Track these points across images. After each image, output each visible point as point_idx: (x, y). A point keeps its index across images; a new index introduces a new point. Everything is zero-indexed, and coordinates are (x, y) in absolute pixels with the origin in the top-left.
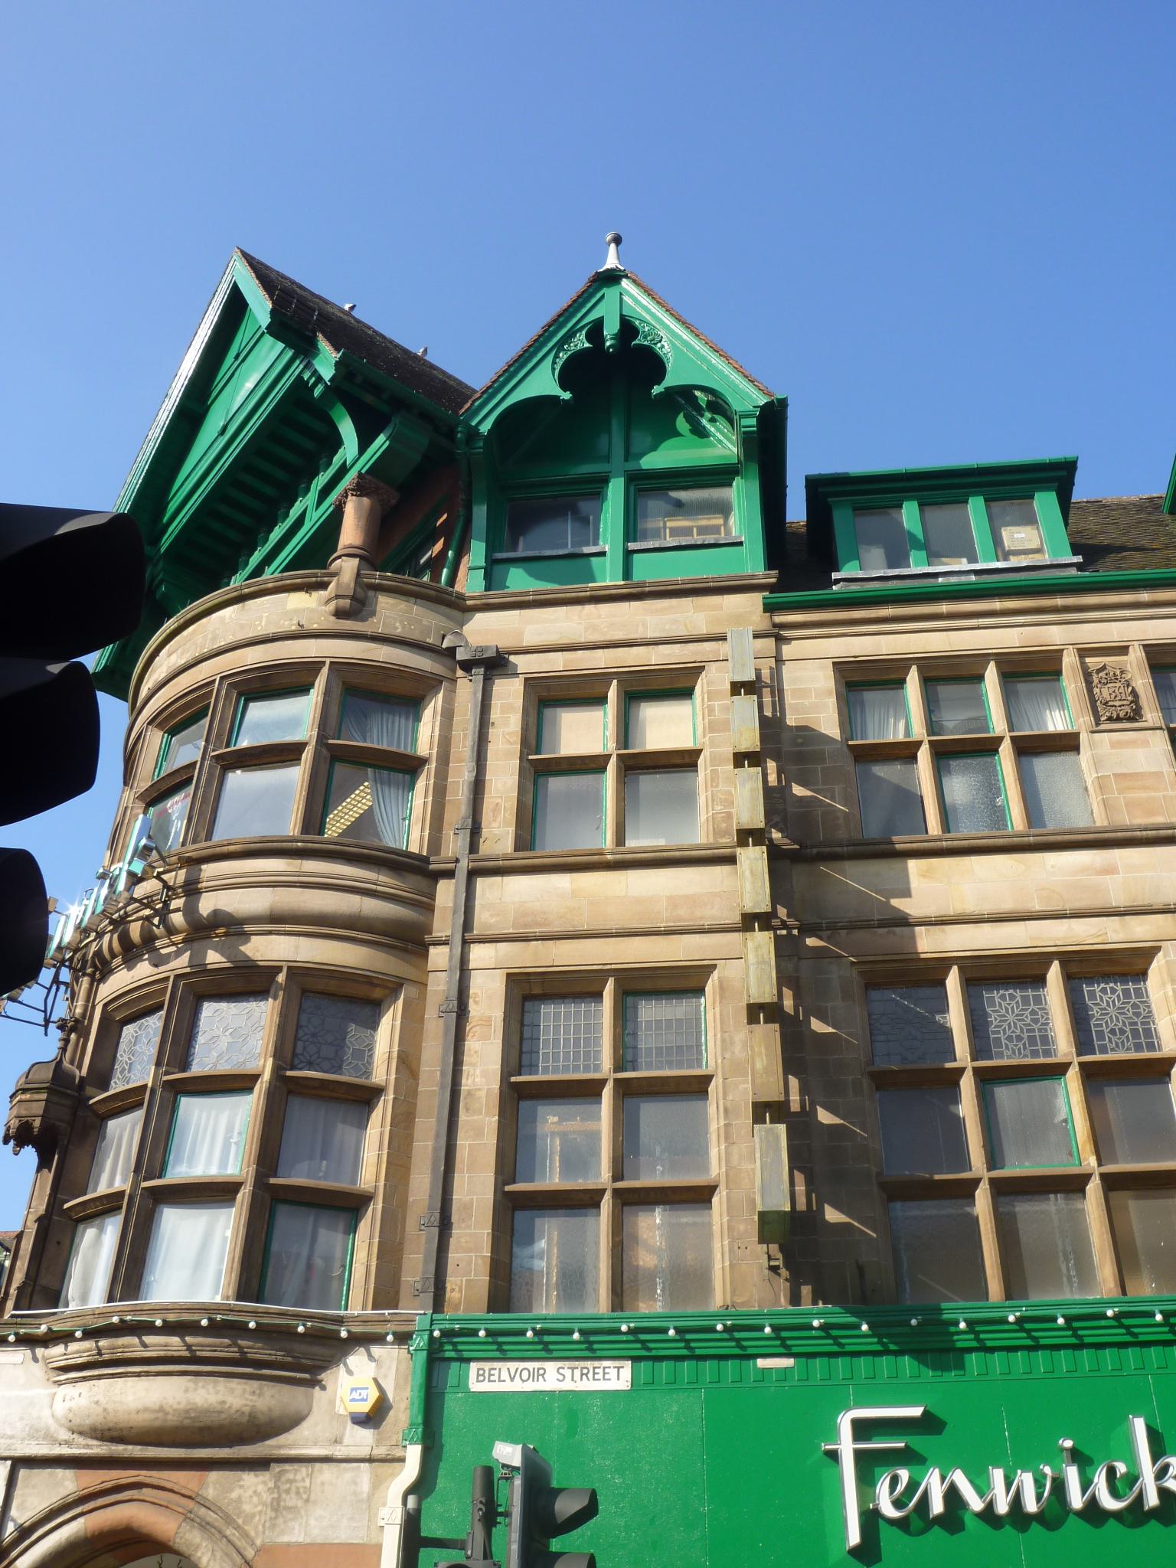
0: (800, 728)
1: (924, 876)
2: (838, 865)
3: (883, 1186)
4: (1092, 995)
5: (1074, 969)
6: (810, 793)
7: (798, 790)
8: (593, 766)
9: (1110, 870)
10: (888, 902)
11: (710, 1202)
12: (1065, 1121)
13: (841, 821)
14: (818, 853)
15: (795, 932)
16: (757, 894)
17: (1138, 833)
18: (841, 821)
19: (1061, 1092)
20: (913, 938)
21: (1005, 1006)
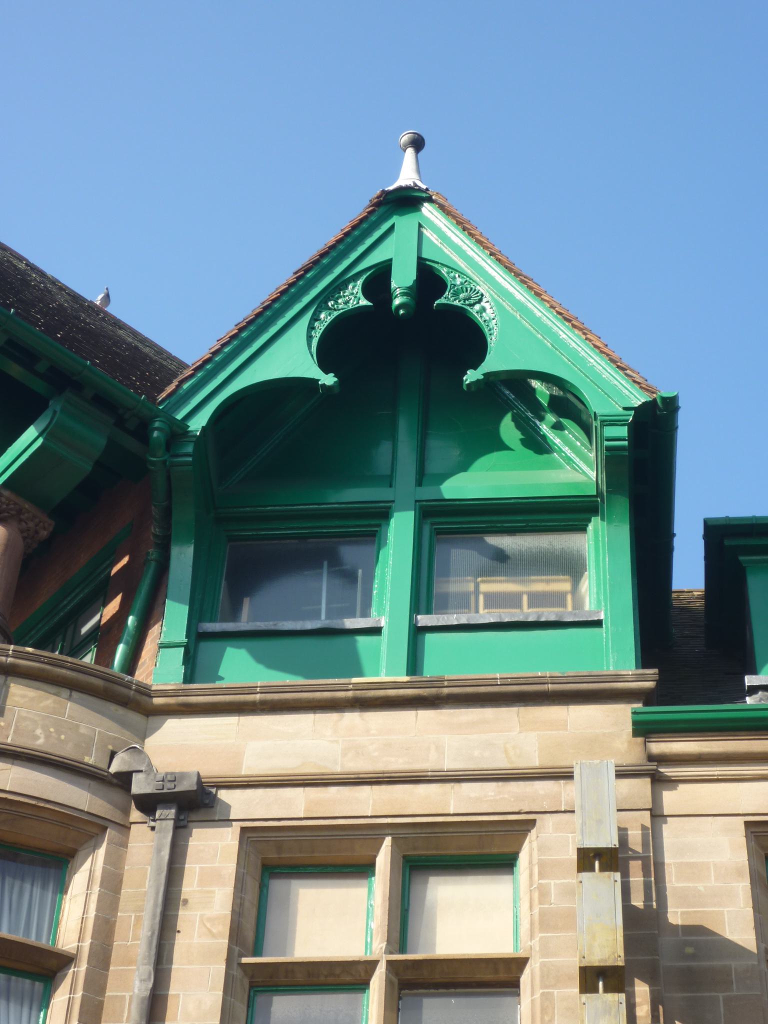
8: (348, 978)
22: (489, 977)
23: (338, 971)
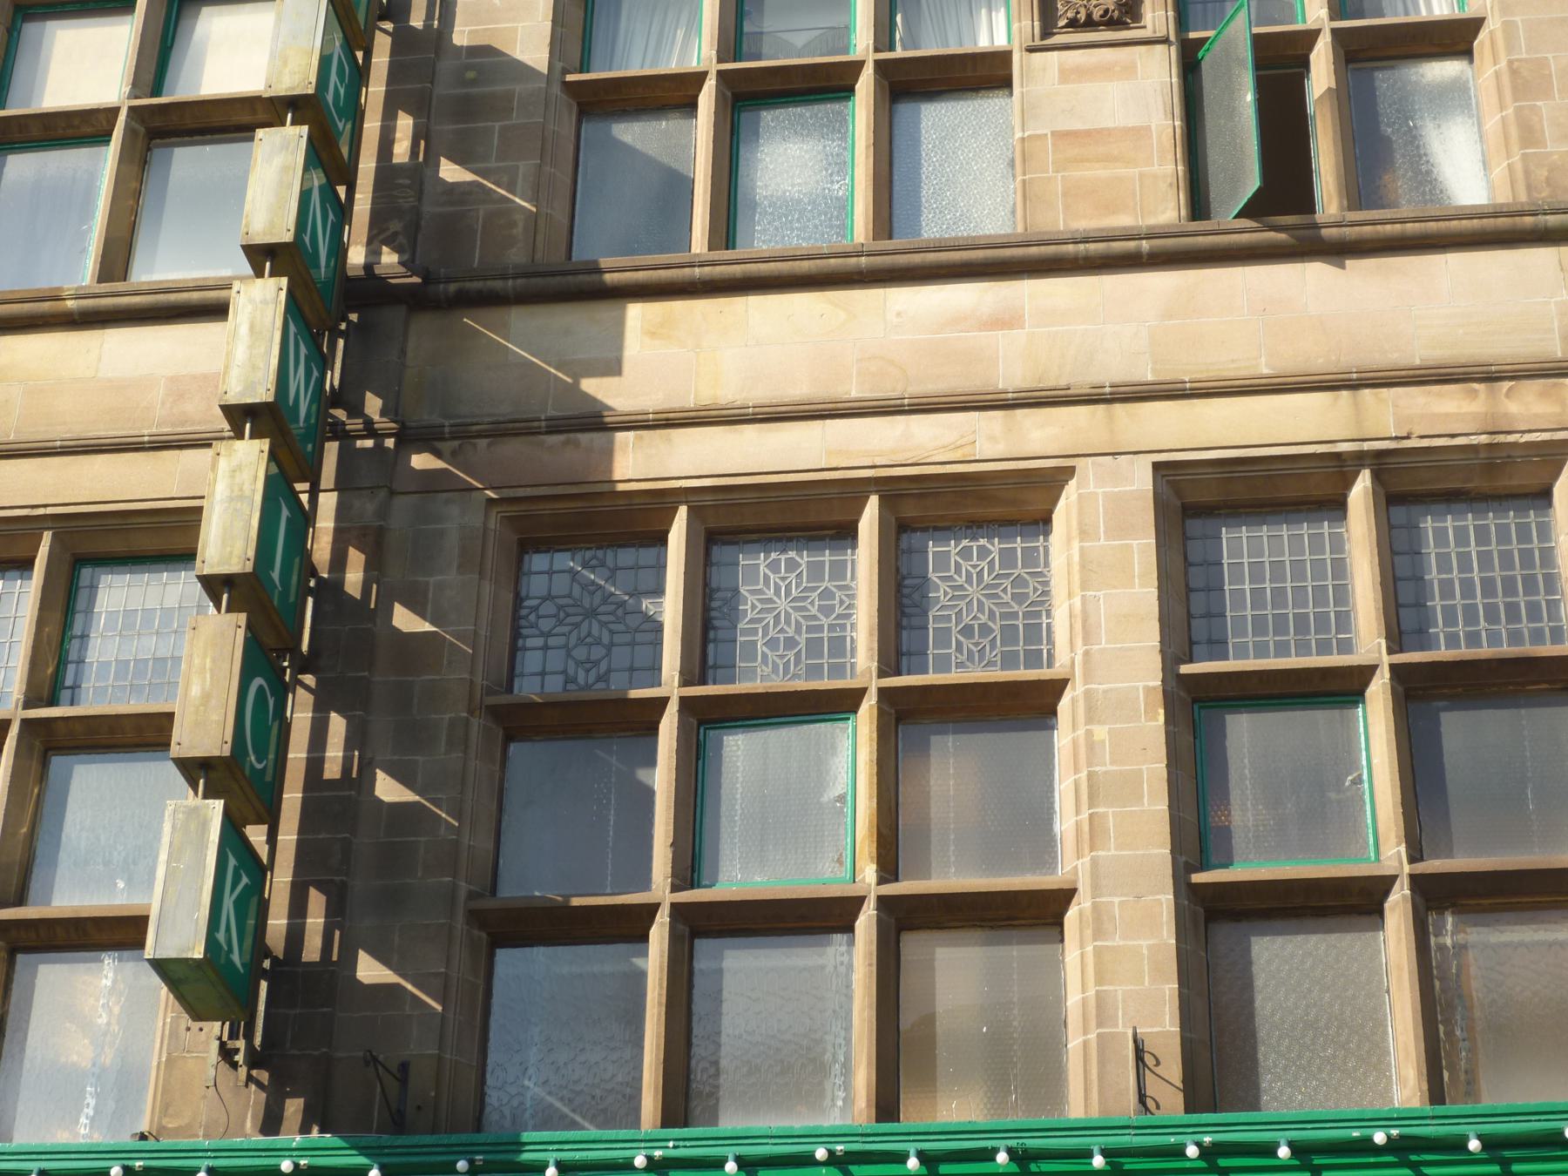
0: (474, 51)
1: (653, 334)
2: (495, 314)
3: (477, 918)
4: (942, 559)
5: (910, 511)
6: (468, 177)
7: (450, 172)
8: (88, 130)
9: (1005, 321)
10: (576, 383)
11: (1060, 924)
12: (841, 798)
13: (519, 231)
14: (460, 292)
15: (390, 443)
16: (254, 368)
17: (1071, 248)
18: (519, 231)
19: (845, 745)
20: (608, 453)
21: (770, 582)
22: (777, 86)
23: (76, 122)
